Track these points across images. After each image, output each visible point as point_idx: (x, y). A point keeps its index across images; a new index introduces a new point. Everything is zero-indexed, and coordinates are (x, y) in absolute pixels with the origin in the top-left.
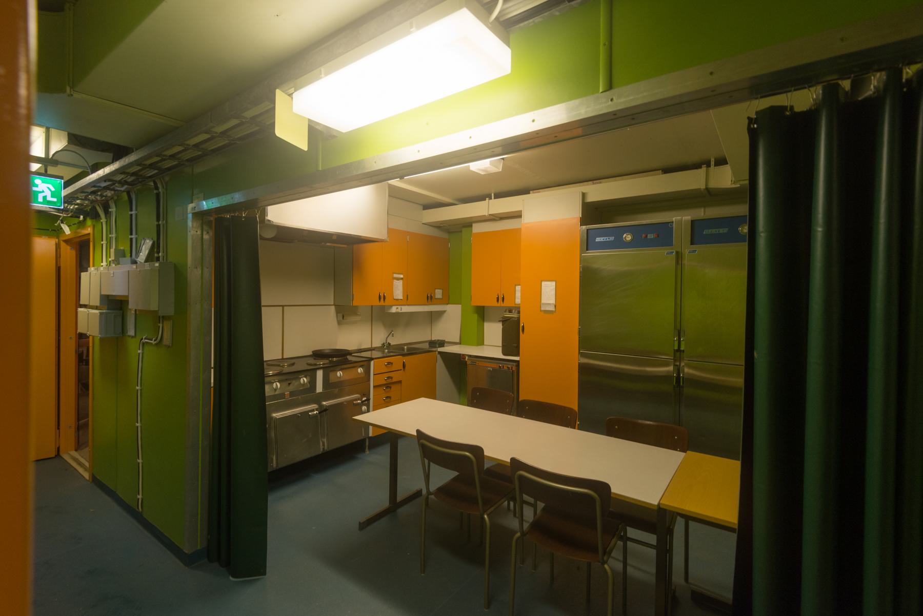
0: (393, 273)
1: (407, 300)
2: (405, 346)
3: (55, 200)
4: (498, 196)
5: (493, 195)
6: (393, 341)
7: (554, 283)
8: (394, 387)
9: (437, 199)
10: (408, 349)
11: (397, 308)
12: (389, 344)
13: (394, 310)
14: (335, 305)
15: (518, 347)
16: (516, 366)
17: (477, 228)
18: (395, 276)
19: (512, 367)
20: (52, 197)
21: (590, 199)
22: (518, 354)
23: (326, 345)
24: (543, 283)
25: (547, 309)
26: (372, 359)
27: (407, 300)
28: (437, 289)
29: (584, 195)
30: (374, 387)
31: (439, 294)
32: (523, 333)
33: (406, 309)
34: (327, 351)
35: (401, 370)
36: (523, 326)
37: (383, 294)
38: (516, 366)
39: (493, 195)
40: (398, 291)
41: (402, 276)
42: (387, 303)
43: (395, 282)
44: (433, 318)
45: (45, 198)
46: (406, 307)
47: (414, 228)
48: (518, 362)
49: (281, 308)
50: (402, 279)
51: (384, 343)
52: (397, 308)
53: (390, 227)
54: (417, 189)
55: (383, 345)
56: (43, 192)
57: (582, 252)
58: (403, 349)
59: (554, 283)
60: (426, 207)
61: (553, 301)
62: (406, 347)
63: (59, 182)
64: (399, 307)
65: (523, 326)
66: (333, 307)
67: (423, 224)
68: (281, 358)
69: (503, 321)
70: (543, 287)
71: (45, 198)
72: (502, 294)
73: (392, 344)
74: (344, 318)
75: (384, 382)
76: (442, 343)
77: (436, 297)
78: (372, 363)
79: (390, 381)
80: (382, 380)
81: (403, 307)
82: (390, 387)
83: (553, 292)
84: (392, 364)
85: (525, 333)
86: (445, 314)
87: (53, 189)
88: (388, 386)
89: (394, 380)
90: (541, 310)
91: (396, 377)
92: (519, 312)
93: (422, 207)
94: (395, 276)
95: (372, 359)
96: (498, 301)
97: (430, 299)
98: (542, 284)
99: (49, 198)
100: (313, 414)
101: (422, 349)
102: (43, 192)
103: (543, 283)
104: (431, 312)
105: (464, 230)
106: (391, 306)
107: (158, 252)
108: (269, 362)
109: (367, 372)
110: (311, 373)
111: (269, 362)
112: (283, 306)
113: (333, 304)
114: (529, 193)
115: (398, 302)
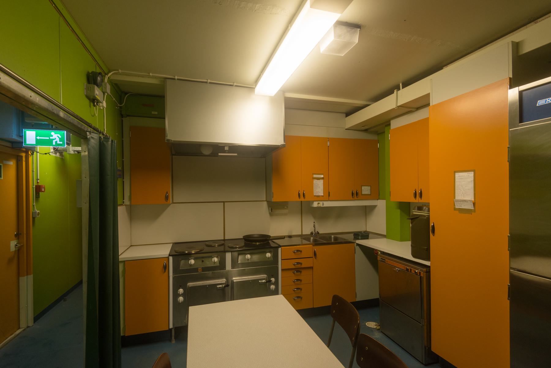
0: (313, 174)
1: (328, 196)
2: (333, 235)
3: (61, 143)
4: (406, 84)
5: (401, 85)
6: (323, 230)
7: (471, 174)
8: (304, 272)
9: (357, 104)
10: (336, 239)
11: (319, 203)
12: (318, 233)
13: (315, 204)
14: (267, 201)
15: (428, 250)
16: (427, 272)
17: (395, 124)
18: (315, 176)
19: (420, 272)
20: (60, 141)
21: (528, 48)
22: (428, 259)
23: (255, 230)
24: (457, 175)
25: (463, 207)
26: (280, 246)
27: (328, 196)
28: (371, 187)
29: (516, 46)
30: (282, 270)
31: (366, 190)
32: (434, 236)
33: (327, 204)
34: (256, 236)
35: (312, 257)
36: (433, 226)
37: (303, 192)
38: (427, 272)
39: (401, 85)
40: (319, 188)
41: (322, 176)
42: (307, 199)
43: (315, 181)
44: (367, 211)
45: (56, 142)
46: (329, 202)
47: (333, 134)
48: (428, 267)
49: (223, 203)
50: (323, 178)
51: (312, 232)
52: (319, 203)
53: (286, 135)
54: (319, 97)
55: (312, 233)
56: (55, 139)
57: (511, 125)
58: (330, 238)
59: (471, 174)
60: (348, 114)
61: (470, 197)
62: (333, 236)
63: (63, 132)
64: (321, 202)
65: (433, 226)
66: (266, 203)
67: (346, 129)
68: (223, 239)
69: (412, 219)
70: (456, 180)
71: (56, 142)
72: (419, 189)
73: (320, 233)
74: (272, 211)
75: (293, 267)
76: (365, 235)
77: (363, 193)
78: (280, 249)
79: (299, 266)
80: (290, 264)
81: (325, 203)
82: (301, 272)
83: (471, 185)
84: (301, 251)
85: (435, 235)
86: (377, 208)
87: (60, 137)
88: (298, 270)
89: (303, 266)
90: (455, 209)
91: (306, 263)
92: (429, 211)
93: (345, 115)
94: (315, 176)
95: (280, 246)
96: (415, 197)
97: (356, 195)
98: (456, 175)
99: (58, 142)
100: (262, 282)
101: (345, 239)
102: (55, 139)
103: (457, 175)
104: (366, 206)
105: (386, 128)
106: (313, 202)
107: (465, 176)
108: (207, 243)
109: (275, 256)
110: (221, 254)
111: (207, 243)
112: (224, 202)
113: (265, 200)
114: (442, 69)
115: (319, 198)
